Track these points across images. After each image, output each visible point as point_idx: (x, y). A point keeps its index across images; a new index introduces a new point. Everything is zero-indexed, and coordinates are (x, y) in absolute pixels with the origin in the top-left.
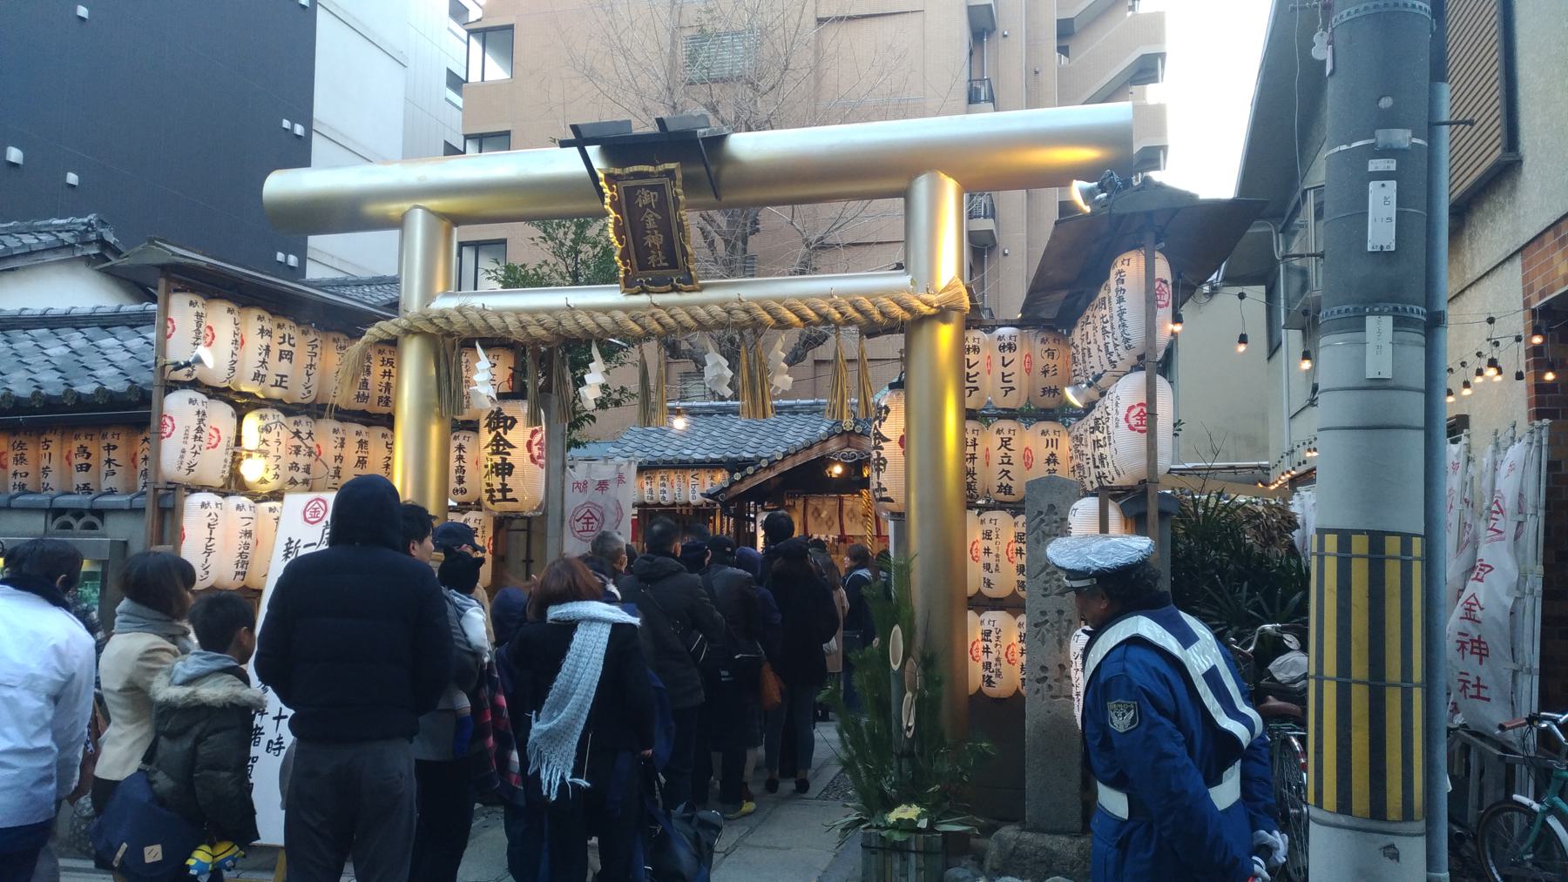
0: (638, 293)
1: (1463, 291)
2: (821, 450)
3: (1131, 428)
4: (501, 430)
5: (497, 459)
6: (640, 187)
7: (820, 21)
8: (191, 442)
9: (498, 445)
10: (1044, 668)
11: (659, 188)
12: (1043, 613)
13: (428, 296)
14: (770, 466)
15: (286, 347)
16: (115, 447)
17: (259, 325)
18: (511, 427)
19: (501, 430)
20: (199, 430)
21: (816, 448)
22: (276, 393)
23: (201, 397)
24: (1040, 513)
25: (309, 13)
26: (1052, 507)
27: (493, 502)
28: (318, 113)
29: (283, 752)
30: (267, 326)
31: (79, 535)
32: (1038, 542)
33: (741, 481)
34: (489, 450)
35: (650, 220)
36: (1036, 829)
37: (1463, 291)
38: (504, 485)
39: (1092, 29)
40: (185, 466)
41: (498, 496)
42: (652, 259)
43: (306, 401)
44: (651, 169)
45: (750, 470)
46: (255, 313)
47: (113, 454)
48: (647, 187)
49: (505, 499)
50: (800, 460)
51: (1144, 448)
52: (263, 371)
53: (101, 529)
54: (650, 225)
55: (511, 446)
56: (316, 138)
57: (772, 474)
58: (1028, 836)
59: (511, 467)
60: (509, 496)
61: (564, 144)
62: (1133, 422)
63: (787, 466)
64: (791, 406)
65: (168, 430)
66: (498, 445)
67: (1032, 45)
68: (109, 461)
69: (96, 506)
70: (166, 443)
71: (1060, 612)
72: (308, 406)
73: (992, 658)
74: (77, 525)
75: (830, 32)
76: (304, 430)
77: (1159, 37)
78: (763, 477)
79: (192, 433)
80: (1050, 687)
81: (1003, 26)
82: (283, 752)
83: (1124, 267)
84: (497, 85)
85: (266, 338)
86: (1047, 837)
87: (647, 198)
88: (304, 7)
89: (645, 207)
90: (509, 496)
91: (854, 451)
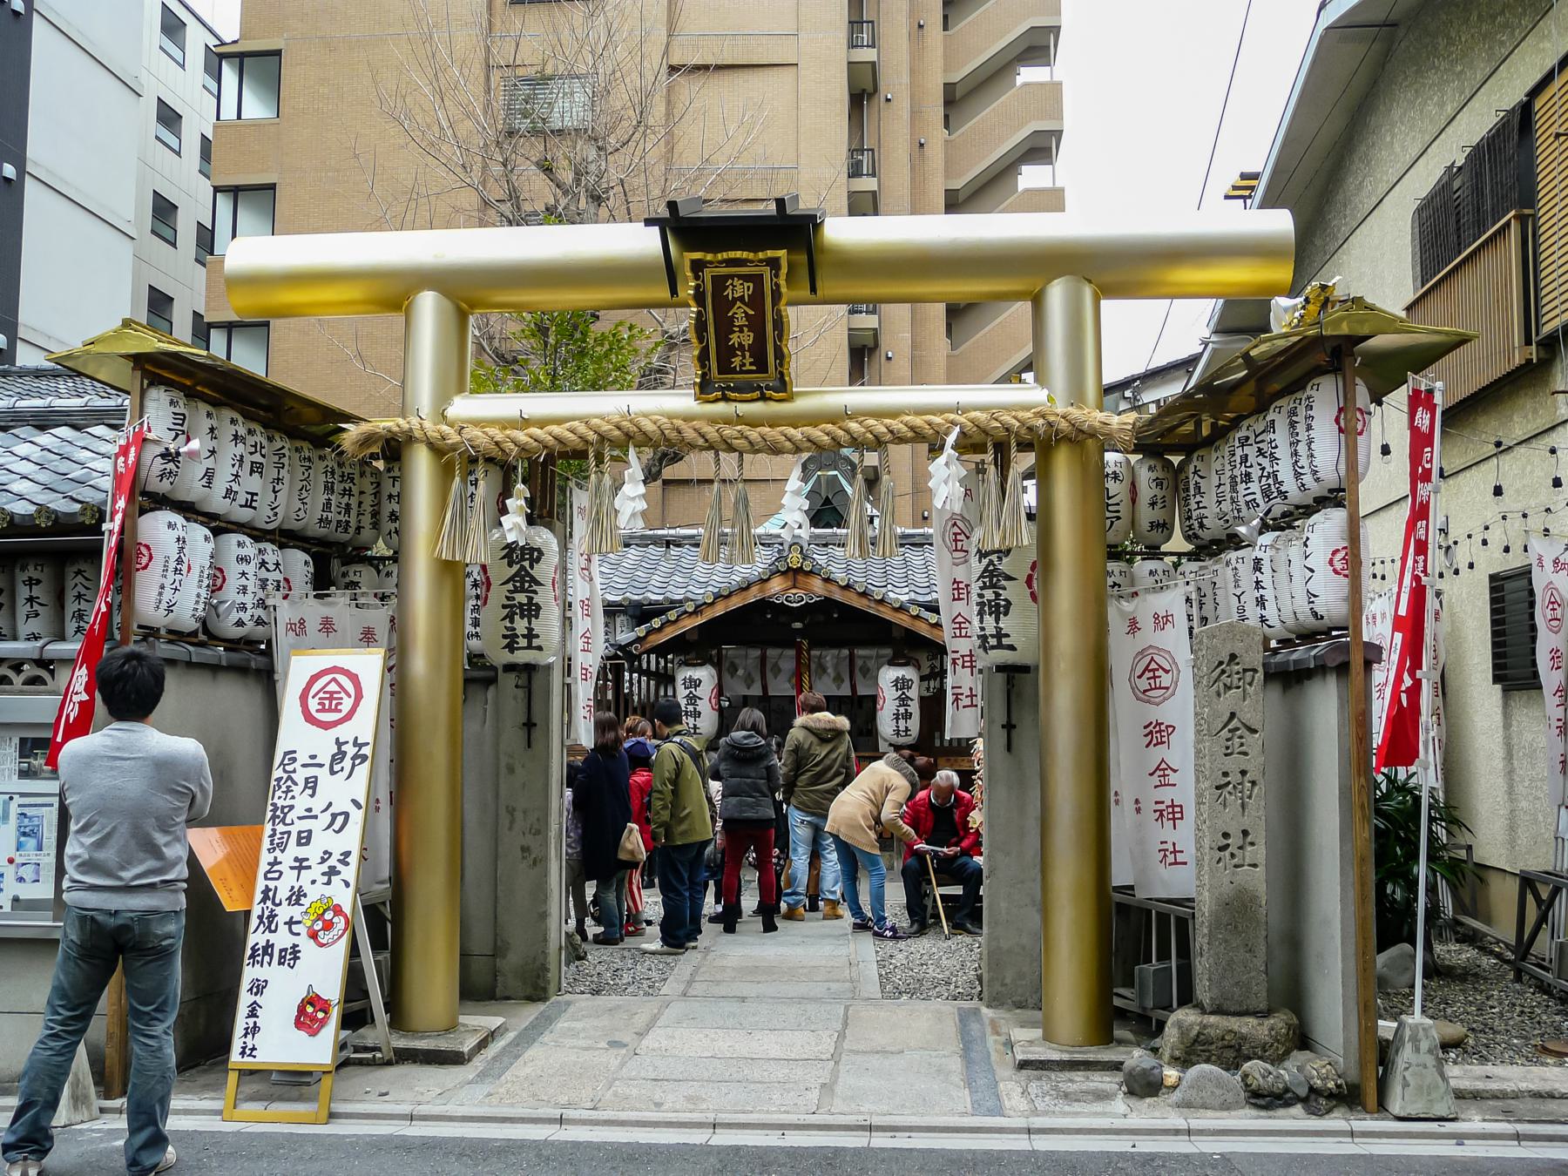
0: (716, 400)
1: (1553, 428)
2: (761, 591)
3: (1335, 571)
4: (526, 564)
5: (989, 594)
6: (732, 277)
7: (673, 69)
8: (170, 574)
9: (991, 577)
10: (1226, 835)
11: (757, 280)
12: (1225, 774)
13: (442, 400)
14: (698, 610)
15: (257, 458)
16: (38, 582)
17: (232, 429)
18: (538, 560)
19: (526, 564)
20: (179, 561)
21: (754, 589)
22: (245, 515)
23: (178, 519)
24: (1221, 663)
25: (21, 22)
26: (1233, 657)
27: (985, 650)
28: (36, 149)
29: (249, 952)
30: (242, 431)
31: (21, 692)
32: (1219, 695)
33: (660, 629)
34: (510, 586)
35: (739, 313)
36: (1219, 1011)
37: (1553, 428)
38: (530, 630)
39: (992, 105)
40: (164, 605)
41: (523, 642)
42: (736, 361)
43: (270, 527)
44: (751, 256)
45: (672, 615)
46: (228, 414)
47: (36, 591)
48: (740, 277)
49: (530, 647)
50: (736, 603)
51: (1346, 591)
52: (235, 487)
53: (51, 684)
54: (740, 321)
55: (538, 583)
56: (30, 185)
57: (700, 620)
58: (1213, 1019)
59: (538, 608)
60: (1005, 641)
61: (649, 222)
62: (1338, 566)
63: (719, 610)
64: (692, 537)
65: (144, 561)
66: (523, 582)
67: (915, 114)
68: (31, 600)
69: (46, 656)
70: (140, 576)
71: (1243, 773)
72: (272, 532)
73: (293, 850)
74: (18, 680)
75: (688, 88)
76: (271, 558)
77: (1058, 114)
78: (689, 624)
79: (172, 565)
80: (1233, 855)
81: (885, 90)
82: (249, 952)
83: (1313, 393)
84: (257, 124)
85: (241, 445)
86: (1233, 1019)
87: (741, 289)
88: (16, 14)
89: (735, 300)
90: (1005, 641)
91: (801, 593)
